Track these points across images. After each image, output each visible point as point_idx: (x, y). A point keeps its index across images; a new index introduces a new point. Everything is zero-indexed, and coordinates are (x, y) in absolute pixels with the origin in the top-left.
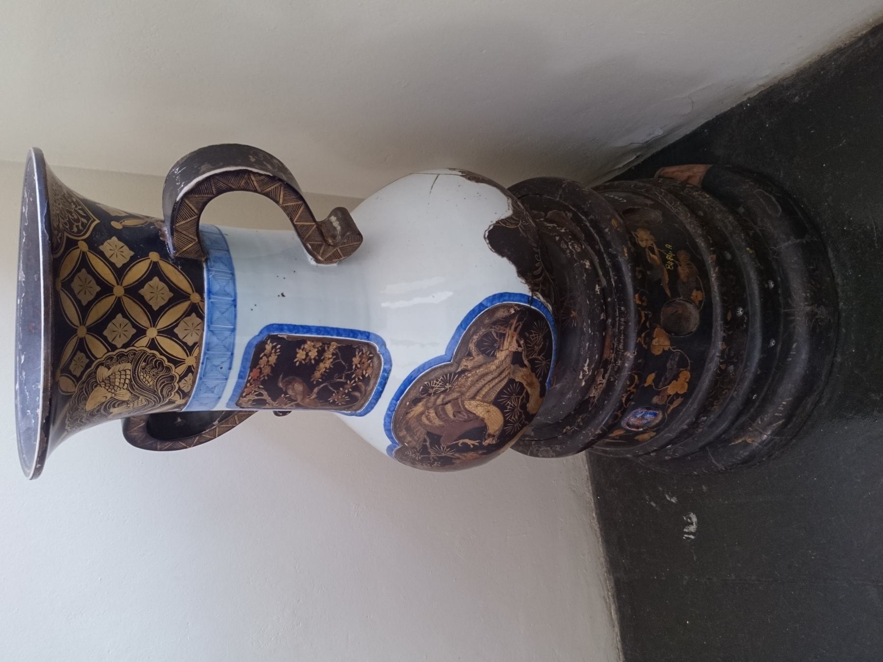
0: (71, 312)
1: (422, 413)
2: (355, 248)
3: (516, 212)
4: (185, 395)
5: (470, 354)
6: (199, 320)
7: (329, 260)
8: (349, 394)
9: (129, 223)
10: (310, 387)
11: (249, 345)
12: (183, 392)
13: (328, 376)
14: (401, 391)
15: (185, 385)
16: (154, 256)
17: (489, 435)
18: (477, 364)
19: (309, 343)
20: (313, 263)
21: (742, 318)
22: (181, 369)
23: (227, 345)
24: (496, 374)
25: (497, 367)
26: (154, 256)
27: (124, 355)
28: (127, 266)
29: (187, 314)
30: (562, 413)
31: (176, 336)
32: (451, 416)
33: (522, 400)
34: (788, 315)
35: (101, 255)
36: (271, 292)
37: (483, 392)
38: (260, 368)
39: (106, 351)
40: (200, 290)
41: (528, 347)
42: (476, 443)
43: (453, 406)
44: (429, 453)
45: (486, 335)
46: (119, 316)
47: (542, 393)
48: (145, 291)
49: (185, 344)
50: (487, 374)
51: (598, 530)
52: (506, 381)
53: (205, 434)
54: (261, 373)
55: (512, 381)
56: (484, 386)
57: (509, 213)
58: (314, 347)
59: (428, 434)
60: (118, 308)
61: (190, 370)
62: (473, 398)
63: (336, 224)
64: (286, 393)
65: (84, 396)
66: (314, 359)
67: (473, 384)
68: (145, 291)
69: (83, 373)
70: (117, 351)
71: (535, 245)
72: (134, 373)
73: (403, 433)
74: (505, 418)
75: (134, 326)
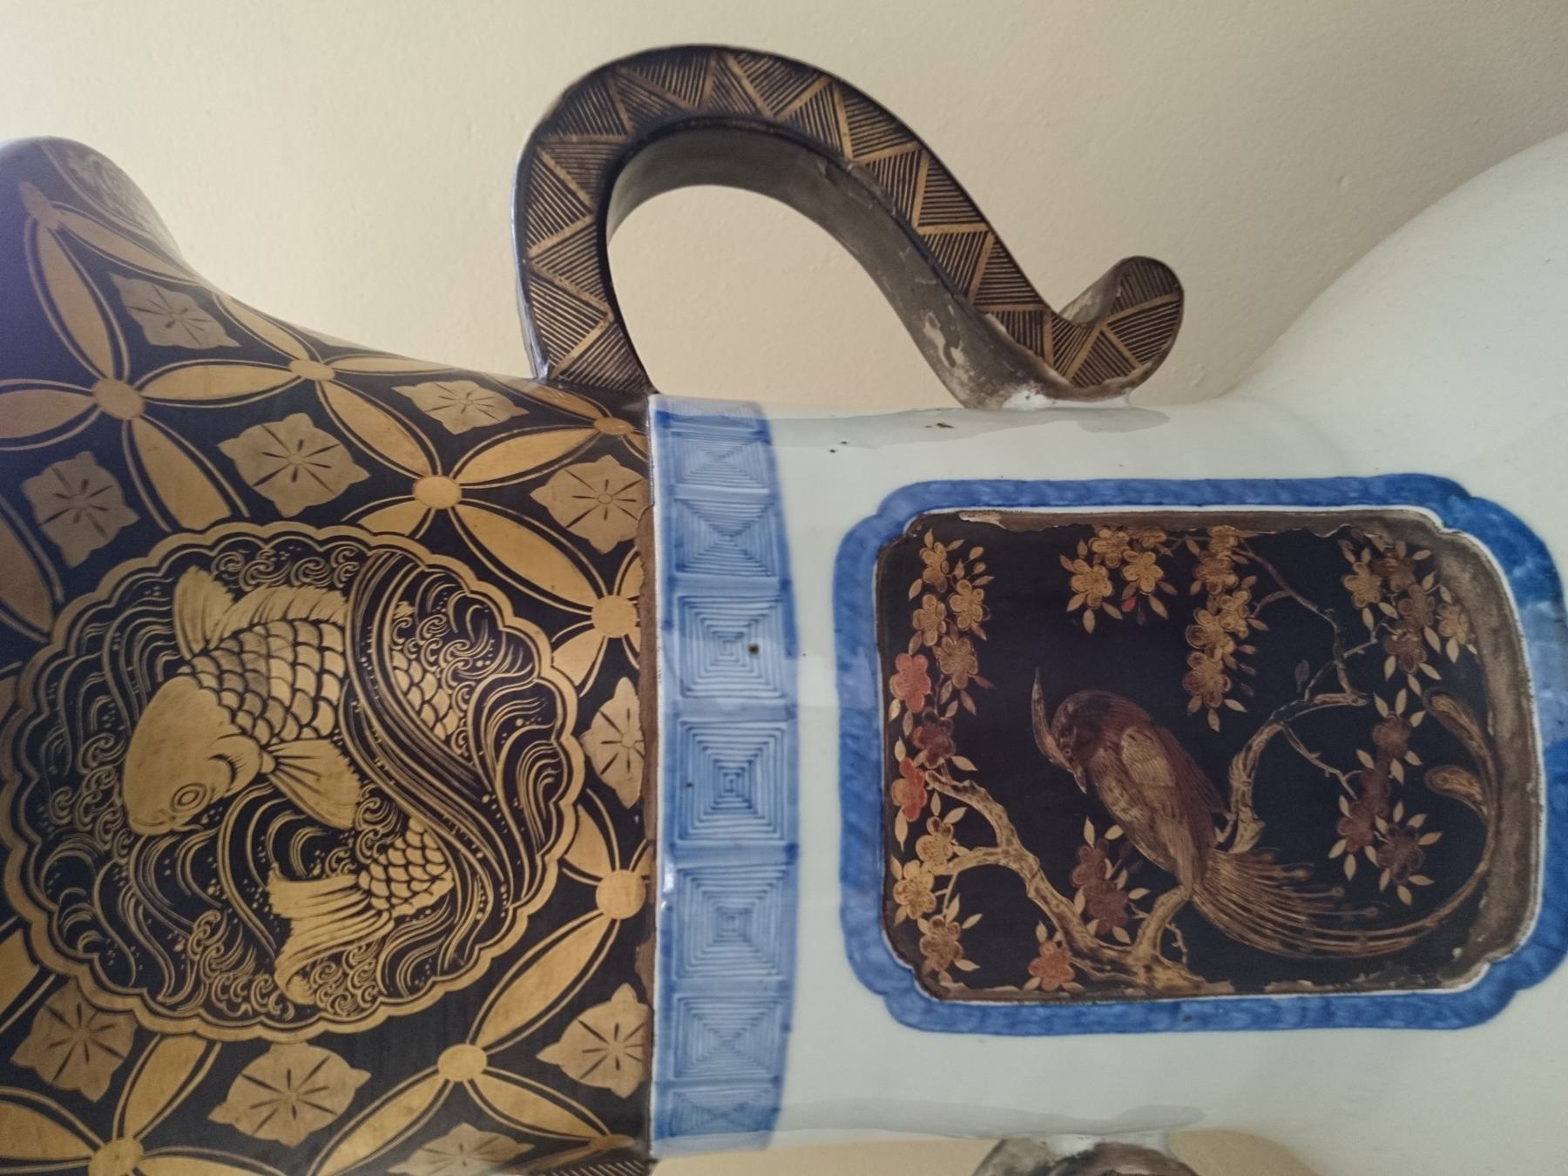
6: (630, 475)
8: (1415, 793)
11: (851, 545)
13: (1262, 675)
19: (1105, 533)
23: (756, 548)
27: (307, 551)
38: (925, 650)
39: (225, 512)
49: (583, 544)
61: (617, 661)
66: (1159, 593)
72: (361, 648)
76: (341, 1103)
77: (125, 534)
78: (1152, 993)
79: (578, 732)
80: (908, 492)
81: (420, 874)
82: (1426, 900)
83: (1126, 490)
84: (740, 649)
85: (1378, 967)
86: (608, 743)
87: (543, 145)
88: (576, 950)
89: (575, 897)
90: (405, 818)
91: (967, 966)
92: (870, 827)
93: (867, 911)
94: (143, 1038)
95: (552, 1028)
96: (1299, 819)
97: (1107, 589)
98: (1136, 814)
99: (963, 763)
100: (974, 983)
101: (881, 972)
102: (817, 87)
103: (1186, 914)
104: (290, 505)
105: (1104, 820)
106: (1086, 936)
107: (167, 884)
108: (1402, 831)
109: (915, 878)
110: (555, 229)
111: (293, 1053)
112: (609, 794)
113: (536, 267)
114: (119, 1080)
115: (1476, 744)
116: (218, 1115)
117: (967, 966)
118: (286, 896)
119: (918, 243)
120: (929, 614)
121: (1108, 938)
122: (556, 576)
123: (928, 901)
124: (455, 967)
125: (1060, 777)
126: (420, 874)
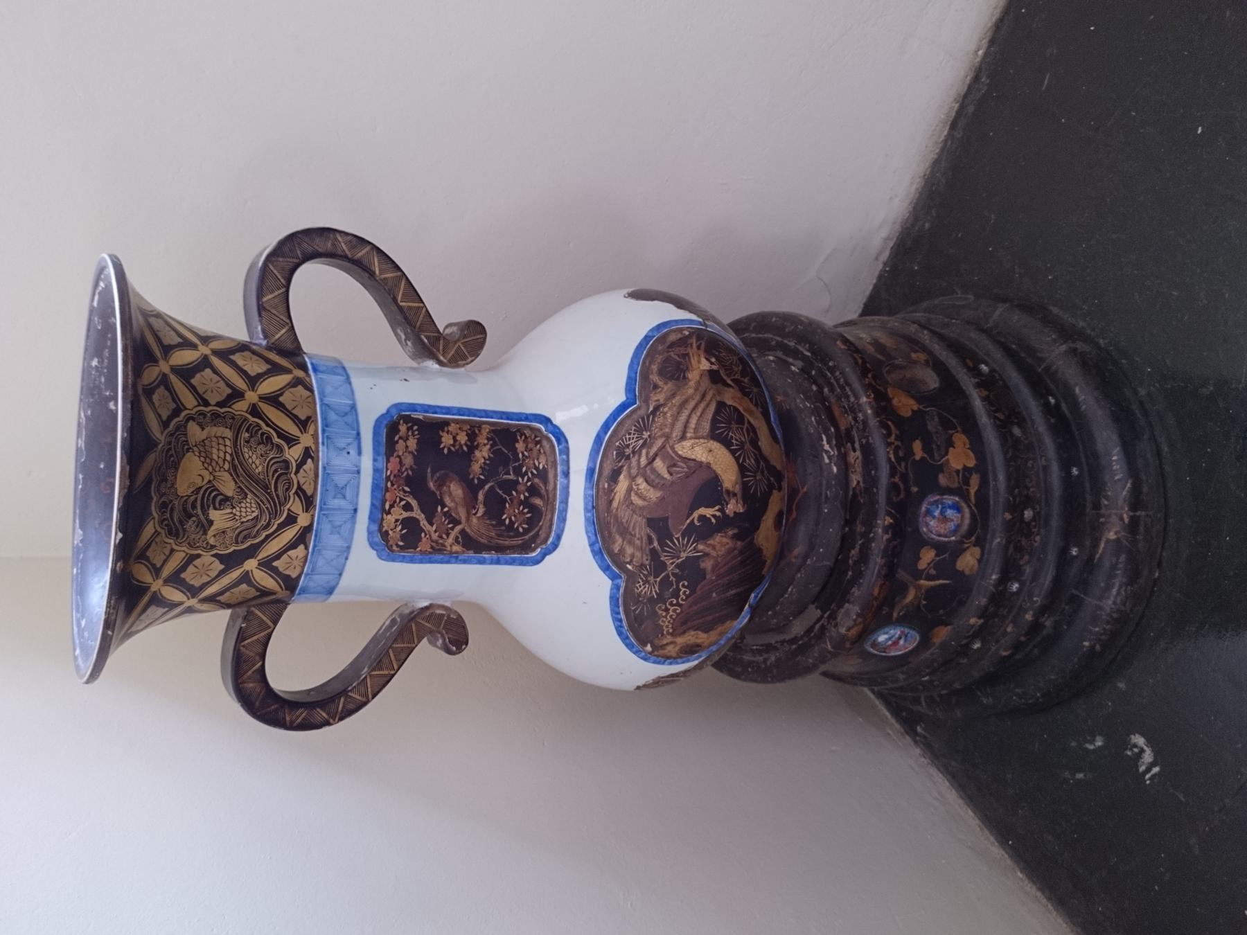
1: (630, 489)
5: (656, 387)
6: (308, 393)
8: (526, 503)
11: (378, 422)
13: (491, 469)
14: (590, 472)
21: (992, 370)
24: (698, 398)
25: (696, 390)
32: (667, 476)
34: (1047, 369)
37: (692, 425)
43: (663, 460)
45: (666, 360)
49: (296, 417)
51: (1039, 894)
61: (308, 454)
67: (676, 418)
70: (210, 408)
72: (235, 445)
76: (213, 574)
77: (174, 410)
78: (451, 553)
79: (296, 473)
80: (395, 406)
81: (249, 510)
82: (526, 531)
83: (461, 411)
84: (345, 453)
85: (512, 549)
86: (303, 478)
87: (272, 262)
88: (290, 534)
89: (291, 520)
90: (246, 497)
91: (401, 543)
92: (378, 504)
93: (375, 527)
94: (172, 551)
95: (278, 556)
96: (495, 507)
97: (452, 442)
98: (452, 505)
99: (407, 489)
100: (402, 548)
101: (377, 544)
102: (368, 248)
103: (463, 532)
104: (213, 402)
105: (444, 506)
106: (435, 536)
107: (185, 510)
108: (522, 513)
109: (390, 519)
110: (272, 292)
111: (207, 558)
112: (304, 492)
113: (266, 306)
114: (165, 561)
115: (543, 491)
116: (183, 575)
117: (401, 543)
118: (214, 514)
119: (400, 308)
120: (401, 446)
121: (441, 537)
122: (292, 429)
123: (392, 526)
124: (255, 537)
125: (434, 494)
126: (249, 510)
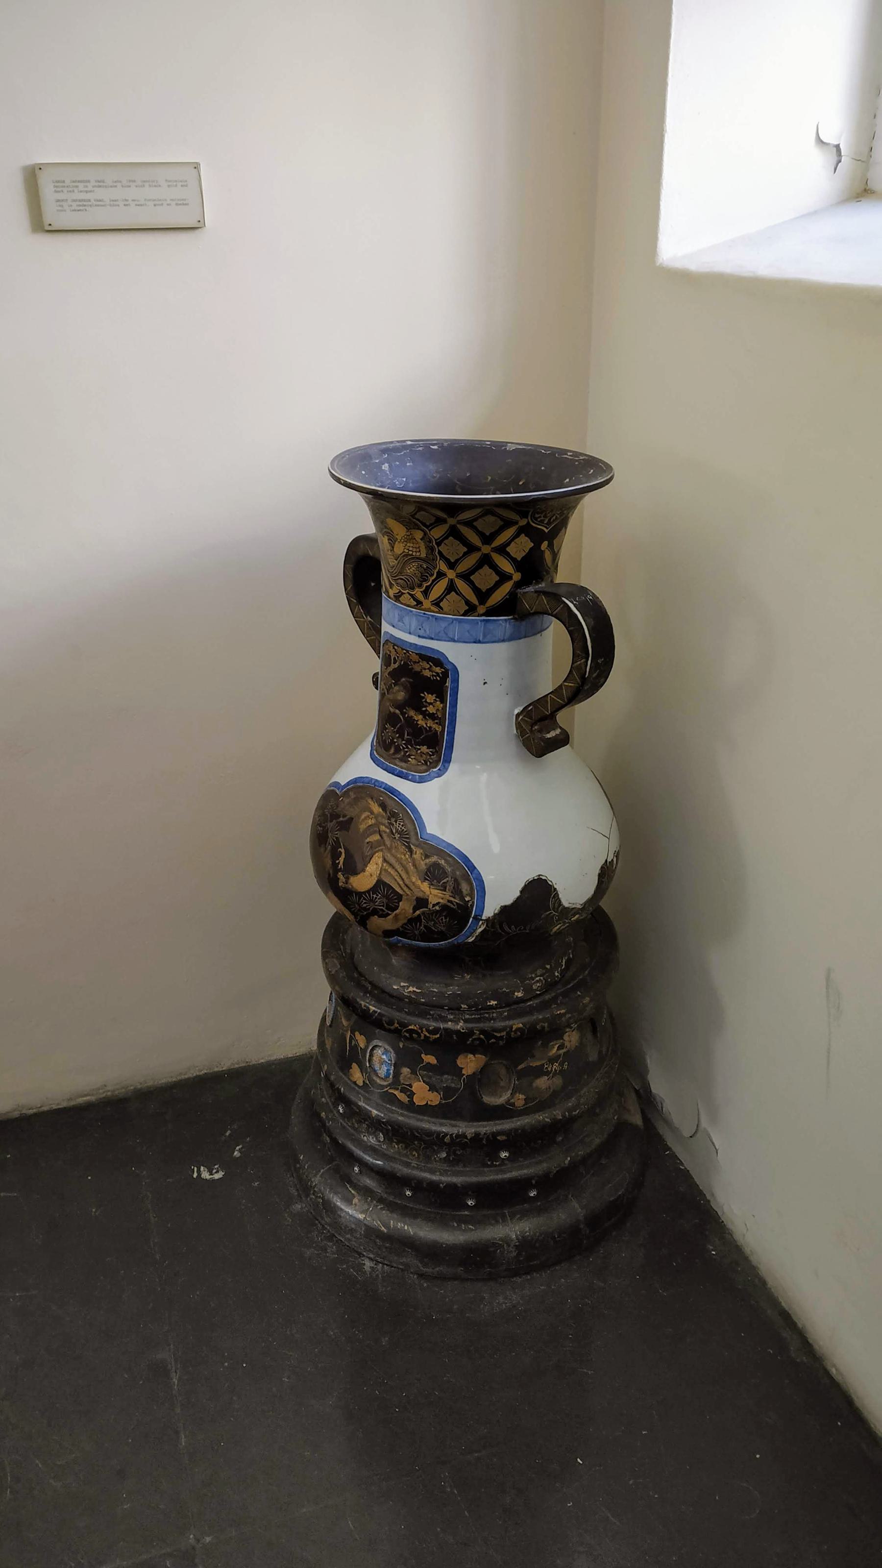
0: (466, 515)
1: (372, 813)
2: (529, 750)
3: (567, 910)
4: (397, 598)
5: (427, 856)
6: (462, 612)
7: (518, 726)
8: (392, 742)
9: (548, 556)
10: (401, 706)
12: (400, 596)
13: (410, 722)
15: (406, 598)
16: (517, 576)
17: (347, 879)
18: (417, 863)
20: (516, 712)
22: (420, 597)
24: (407, 882)
26: (517, 576)
28: (507, 555)
29: (468, 602)
30: (364, 967)
31: (448, 593)
32: (368, 840)
33: (382, 910)
35: (516, 536)
36: (487, 675)
40: (490, 612)
41: (432, 914)
42: (341, 865)
44: (331, 821)
45: (445, 874)
46: (465, 549)
47: (388, 933)
48: (486, 569)
49: (442, 600)
50: (407, 873)
51: (186, 1077)
52: (401, 892)
53: (359, 609)
54: (415, 662)
55: (400, 898)
56: (396, 870)
57: (566, 904)
58: (438, 710)
59: (352, 819)
60: (472, 549)
61: (419, 603)
62: (385, 860)
63: (552, 734)
64: (395, 684)
65: (399, 519)
67: (399, 860)
68: (486, 569)
69: (418, 520)
71: (533, 927)
73: (352, 795)
74: (364, 893)
75: (457, 561)
113: (540, 598)
